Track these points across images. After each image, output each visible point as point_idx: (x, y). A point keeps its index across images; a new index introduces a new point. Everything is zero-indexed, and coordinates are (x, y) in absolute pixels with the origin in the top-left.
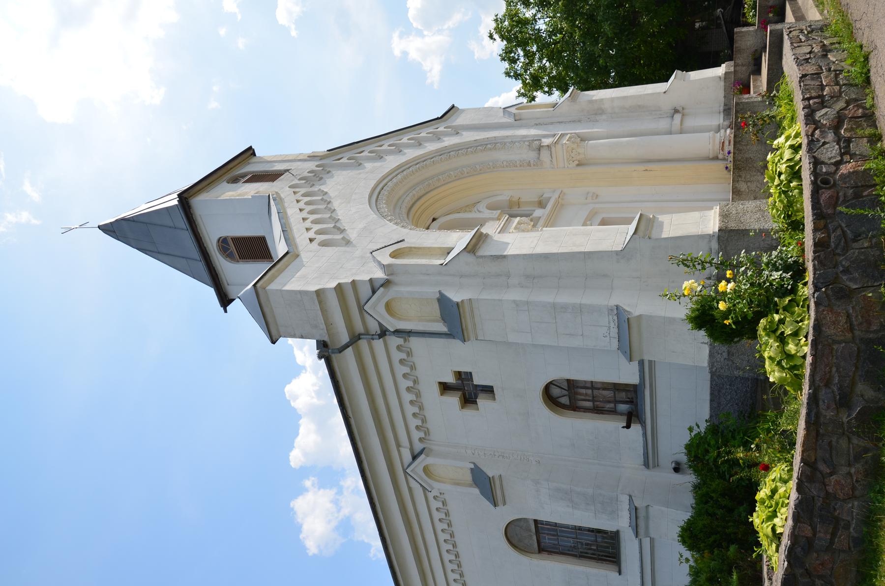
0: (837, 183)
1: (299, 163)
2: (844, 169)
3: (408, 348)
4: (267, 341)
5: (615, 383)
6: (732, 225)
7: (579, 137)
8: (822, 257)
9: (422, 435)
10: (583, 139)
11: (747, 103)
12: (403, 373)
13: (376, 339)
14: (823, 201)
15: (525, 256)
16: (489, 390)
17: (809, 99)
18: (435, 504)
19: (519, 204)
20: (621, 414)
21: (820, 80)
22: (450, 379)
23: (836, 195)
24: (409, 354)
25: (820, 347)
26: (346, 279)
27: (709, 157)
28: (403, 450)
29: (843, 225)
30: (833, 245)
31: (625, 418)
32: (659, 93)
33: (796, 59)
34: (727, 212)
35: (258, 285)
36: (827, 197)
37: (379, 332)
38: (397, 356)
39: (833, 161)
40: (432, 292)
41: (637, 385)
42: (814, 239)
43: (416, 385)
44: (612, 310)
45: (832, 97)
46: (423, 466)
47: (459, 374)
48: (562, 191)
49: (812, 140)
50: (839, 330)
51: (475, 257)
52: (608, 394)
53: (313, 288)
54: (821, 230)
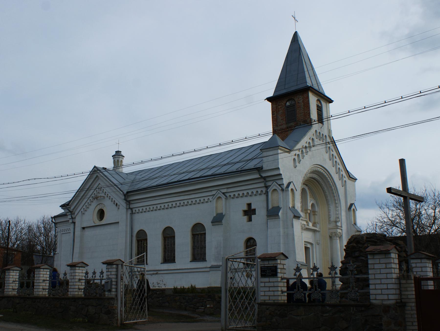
7: (341, 236)
9: (232, 196)
10: (341, 237)
15: (293, 233)
16: (250, 220)
18: (206, 199)
19: (314, 215)
22: (253, 207)
28: (226, 189)
35: (280, 147)
37: (267, 185)
38: (259, 190)
40: (281, 205)
47: (255, 210)
48: (320, 231)
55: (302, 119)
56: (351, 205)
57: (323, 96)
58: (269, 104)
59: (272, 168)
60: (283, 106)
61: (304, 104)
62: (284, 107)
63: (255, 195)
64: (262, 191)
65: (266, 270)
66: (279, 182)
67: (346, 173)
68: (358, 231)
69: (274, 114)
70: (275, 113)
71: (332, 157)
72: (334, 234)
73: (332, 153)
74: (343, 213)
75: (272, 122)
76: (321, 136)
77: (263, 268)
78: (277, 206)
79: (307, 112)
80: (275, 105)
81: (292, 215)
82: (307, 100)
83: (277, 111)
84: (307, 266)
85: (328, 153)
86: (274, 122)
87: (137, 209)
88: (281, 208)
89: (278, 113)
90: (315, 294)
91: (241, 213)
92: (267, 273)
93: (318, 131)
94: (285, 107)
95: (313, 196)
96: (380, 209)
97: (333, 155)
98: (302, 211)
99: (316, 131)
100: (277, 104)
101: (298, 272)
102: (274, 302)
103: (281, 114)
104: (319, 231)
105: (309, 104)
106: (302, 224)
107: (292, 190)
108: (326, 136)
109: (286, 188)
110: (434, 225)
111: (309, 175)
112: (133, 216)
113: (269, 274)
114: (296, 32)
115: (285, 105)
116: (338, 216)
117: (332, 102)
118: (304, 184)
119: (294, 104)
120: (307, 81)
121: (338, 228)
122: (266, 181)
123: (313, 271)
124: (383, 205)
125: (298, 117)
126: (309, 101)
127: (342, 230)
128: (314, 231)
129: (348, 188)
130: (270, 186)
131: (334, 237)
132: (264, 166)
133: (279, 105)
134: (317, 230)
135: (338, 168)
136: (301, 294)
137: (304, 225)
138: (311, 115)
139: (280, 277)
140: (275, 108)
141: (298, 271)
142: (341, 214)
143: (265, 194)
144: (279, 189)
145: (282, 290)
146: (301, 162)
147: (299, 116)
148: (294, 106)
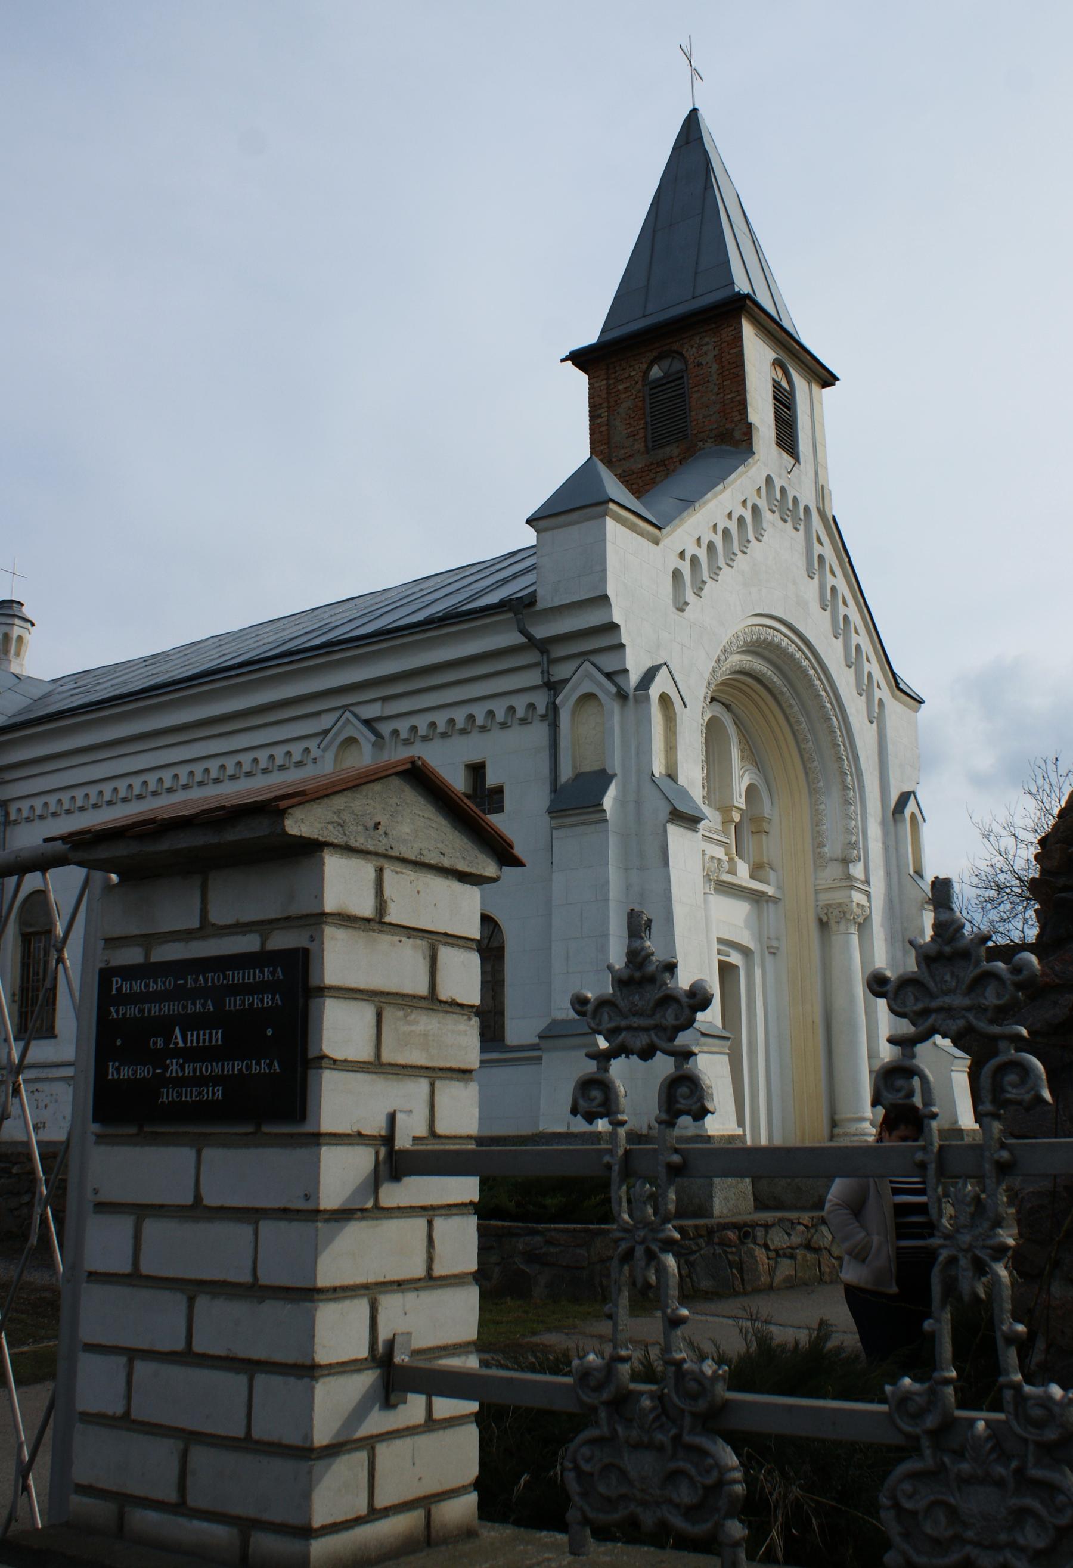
2: (760, 1254)
3: (532, 719)
7: (865, 920)
9: (404, 735)
10: (864, 926)
13: (543, 677)
18: (297, 750)
19: (759, 832)
22: (492, 779)
23: (732, 1244)
28: (378, 705)
29: (702, 1252)
35: (612, 506)
37: (553, 679)
38: (520, 703)
40: (616, 765)
41: (504, 1040)
43: (478, 729)
46: (357, 737)
47: (499, 791)
48: (780, 899)
49: (793, 1223)
54: (696, 1232)
55: (711, 430)
56: (904, 798)
57: (797, 347)
58: (581, 380)
60: (637, 383)
61: (723, 367)
62: (639, 386)
63: (504, 725)
64: (531, 706)
65: (164, 1025)
66: (609, 663)
69: (600, 416)
70: (603, 410)
71: (829, 599)
72: (836, 912)
73: (830, 581)
74: (874, 831)
75: (591, 448)
76: (791, 506)
77: (123, 999)
79: (732, 398)
80: (602, 380)
81: (664, 811)
82: (732, 351)
84: (729, 1043)
85: (816, 577)
86: (598, 449)
87: (25, 805)
90: (965, 1481)
92: (174, 1068)
93: (778, 483)
94: (643, 386)
95: (754, 756)
96: (986, 840)
97: (834, 589)
98: (708, 798)
99: (769, 480)
100: (613, 376)
101: (646, 1054)
102: (244, 1557)
103: (627, 414)
104: (775, 900)
105: (742, 365)
106: (707, 857)
107: (664, 699)
108: (807, 509)
109: (637, 689)
111: (737, 660)
112: (7, 836)
113: (200, 1081)
114: (694, 112)
115: (643, 376)
116: (854, 838)
117: (834, 385)
118: (713, 699)
119: (681, 371)
120: (735, 282)
121: (852, 887)
122: (552, 662)
123: (924, 1037)
124: (994, 824)
125: (695, 423)
126: (740, 354)
127: (868, 895)
128: (757, 898)
129: (890, 733)
130: (567, 681)
131: (838, 923)
132: (540, 593)
133: (619, 378)
134: (770, 894)
135: (854, 644)
136: (704, 1453)
137: (715, 861)
138: (750, 409)
139: (358, 1138)
140: (604, 394)
141: (641, 1041)
143: (543, 717)
144: (607, 692)
145: (391, 1344)
146: (703, 593)
147: (701, 417)
148: (682, 377)
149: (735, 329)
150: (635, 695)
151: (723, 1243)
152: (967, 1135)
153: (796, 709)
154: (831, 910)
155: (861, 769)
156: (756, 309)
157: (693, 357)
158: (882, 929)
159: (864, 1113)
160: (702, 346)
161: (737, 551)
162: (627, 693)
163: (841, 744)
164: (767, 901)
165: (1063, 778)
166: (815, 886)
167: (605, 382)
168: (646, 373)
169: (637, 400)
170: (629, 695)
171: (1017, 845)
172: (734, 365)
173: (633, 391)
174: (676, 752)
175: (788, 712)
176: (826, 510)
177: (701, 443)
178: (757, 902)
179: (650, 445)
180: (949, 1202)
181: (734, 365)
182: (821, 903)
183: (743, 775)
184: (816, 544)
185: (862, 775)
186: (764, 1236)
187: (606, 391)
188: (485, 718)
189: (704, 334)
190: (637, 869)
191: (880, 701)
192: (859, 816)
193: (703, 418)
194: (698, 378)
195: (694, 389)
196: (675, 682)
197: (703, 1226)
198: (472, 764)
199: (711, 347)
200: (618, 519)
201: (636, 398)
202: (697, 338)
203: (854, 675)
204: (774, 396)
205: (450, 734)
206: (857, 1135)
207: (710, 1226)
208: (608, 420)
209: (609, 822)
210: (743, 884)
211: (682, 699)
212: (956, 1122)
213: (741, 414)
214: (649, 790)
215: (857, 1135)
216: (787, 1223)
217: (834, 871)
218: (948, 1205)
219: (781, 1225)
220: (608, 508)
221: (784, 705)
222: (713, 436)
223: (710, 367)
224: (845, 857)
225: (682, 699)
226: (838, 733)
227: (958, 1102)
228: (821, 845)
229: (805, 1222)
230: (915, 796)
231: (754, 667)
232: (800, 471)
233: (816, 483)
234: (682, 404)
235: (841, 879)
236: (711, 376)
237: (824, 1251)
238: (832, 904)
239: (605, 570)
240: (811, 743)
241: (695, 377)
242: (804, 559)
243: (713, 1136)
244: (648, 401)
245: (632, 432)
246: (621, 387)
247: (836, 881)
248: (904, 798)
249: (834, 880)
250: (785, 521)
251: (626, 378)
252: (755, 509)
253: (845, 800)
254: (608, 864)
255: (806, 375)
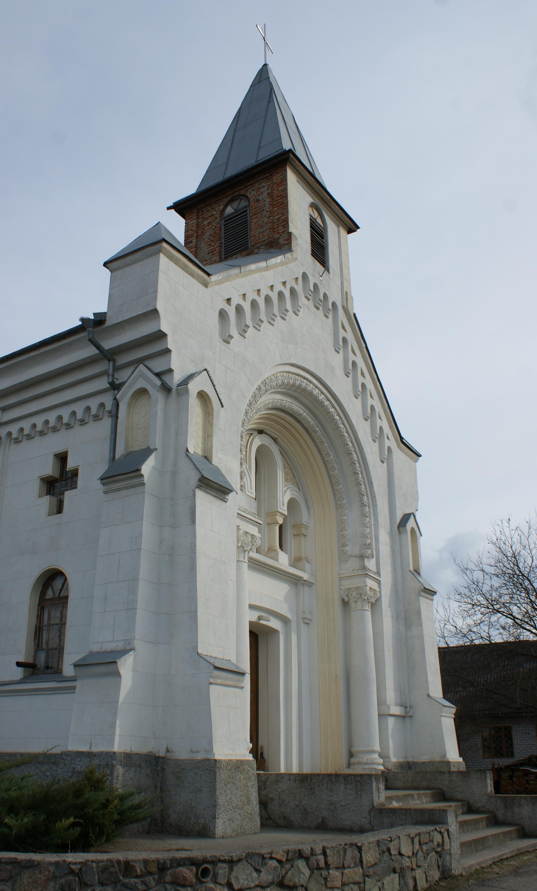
0: (204, 885)
1: (339, 283)
4: (106, 259)
5: (64, 649)
6: (222, 775)
7: (376, 601)
8: (112, 870)
10: (375, 605)
11: (371, 787)
12: (77, 412)
13: (108, 379)
14: (181, 870)
15: (193, 545)
17: (324, 853)
20: (35, 657)
21: (352, 865)
22: (71, 465)
23: (187, 884)
24: (97, 418)
25: (9, 867)
26: (171, 345)
27: (352, 747)
30: (127, 880)
31: (31, 661)
32: (428, 689)
33: (390, 839)
34: (242, 768)
35: (164, 245)
36: (185, 875)
39: (233, 881)
40: (157, 442)
41: (61, 673)
42: (135, 861)
44: (129, 644)
45: (326, 879)
47: (75, 473)
48: (313, 584)
49: (264, 858)
50: (27, 888)
51: (194, 487)
52: (54, 643)
53: (160, 306)
54: (145, 868)
56: (406, 518)
59: (135, 314)
60: (216, 218)
63: (83, 422)
66: (158, 365)
67: (391, 427)
68: (425, 588)
69: (191, 242)
70: (193, 238)
72: (354, 594)
73: (352, 357)
74: (384, 537)
78: (145, 447)
80: (194, 220)
81: (194, 478)
82: (280, 188)
83: (200, 234)
88: (156, 449)
89: (202, 239)
91: (36, 486)
99: (305, 276)
100: (201, 217)
104: (310, 584)
108: (334, 304)
110: (521, 667)
111: (279, 399)
114: (265, 65)
115: (221, 214)
116: (369, 541)
119: (246, 207)
121: (367, 575)
122: (116, 369)
125: (253, 238)
126: (285, 190)
127: (379, 582)
133: (205, 217)
134: (305, 578)
137: (249, 536)
138: (290, 224)
140: (194, 228)
142: (377, 539)
144: (153, 385)
146: (247, 335)
147: (257, 233)
149: (282, 175)
150: (177, 390)
151: (177, 882)
152: (453, 766)
153: (326, 444)
154: (350, 593)
155: (374, 492)
156: (297, 162)
157: (254, 197)
158: (389, 609)
159: (373, 747)
160: (260, 188)
161: (277, 313)
162: (171, 388)
163: (360, 473)
164: (303, 585)
165: (514, 531)
166: (339, 575)
167: (196, 220)
168: (223, 211)
169: (216, 229)
170: (172, 389)
171: (484, 576)
172: (281, 197)
173: (213, 224)
174: (212, 440)
175: (320, 447)
176: (349, 308)
177: (257, 249)
178: (296, 584)
179: (223, 257)
180: (436, 829)
181: (281, 197)
182: (343, 588)
183: (285, 491)
184: (341, 330)
185: (375, 497)
186: (227, 874)
187: (196, 226)
188: (69, 418)
189: (262, 181)
190: (170, 526)
191: (389, 448)
192: (373, 526)
193: (259, 234)
194: (257, 209)
195: (253, 217)
196: (214, 386)
197: (153, 861)
198: (59, 454)
199: (266, 188)
200: (171, 258)
201: (216, 228)
202: (257, 185)
203: (369, 427)
204: (311, 225)
205: (46, 432)
206: (368, 764)
207: (162, 861)
208: (196, 244)
209: (146, 485)
210: (283, 568)
211: (220, 400)
212: (445, 756)
213: (284, 228)
214: (184, 462)
215: (368, 764)
216: (257, 858)
217: (353, 564)
218: (436, 832)
219: (249, 861)
220: (162, 246)
221: (317, 441)
222: (265, 244)
223: (265, 201)
224: (362, 555)
225: (220, 400)
226: (358, 465)
227: (446, 740)
228: (344, 545)
229: (278, 857)
230: (414, 517)
231: (293, 407)
232: (330, 278)
233: (342, 290)
234: (246, 227)
235: (358, 569)
236: (265, 206)
237: (299, 888)
238: (350, 588)
239: (156, 291)
240: (337, 470)
241: (255, 209)
242: (332, 338)
243: (220, 761)
244: (223, 229)
245: (212, 249)
246: (206, 223)
247: (355, 571)
248: (406, 518)
249: (353, 570)
250: (318, 309)
251: (210, 217)
252: (293, 291)
253: (363, 514)
254: (143, 520)
255: (335, 220)
